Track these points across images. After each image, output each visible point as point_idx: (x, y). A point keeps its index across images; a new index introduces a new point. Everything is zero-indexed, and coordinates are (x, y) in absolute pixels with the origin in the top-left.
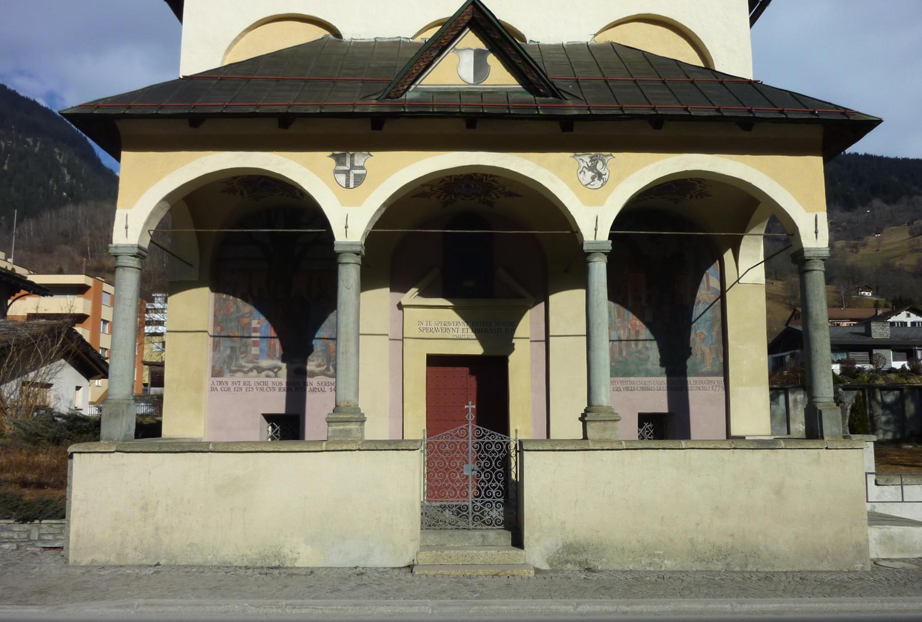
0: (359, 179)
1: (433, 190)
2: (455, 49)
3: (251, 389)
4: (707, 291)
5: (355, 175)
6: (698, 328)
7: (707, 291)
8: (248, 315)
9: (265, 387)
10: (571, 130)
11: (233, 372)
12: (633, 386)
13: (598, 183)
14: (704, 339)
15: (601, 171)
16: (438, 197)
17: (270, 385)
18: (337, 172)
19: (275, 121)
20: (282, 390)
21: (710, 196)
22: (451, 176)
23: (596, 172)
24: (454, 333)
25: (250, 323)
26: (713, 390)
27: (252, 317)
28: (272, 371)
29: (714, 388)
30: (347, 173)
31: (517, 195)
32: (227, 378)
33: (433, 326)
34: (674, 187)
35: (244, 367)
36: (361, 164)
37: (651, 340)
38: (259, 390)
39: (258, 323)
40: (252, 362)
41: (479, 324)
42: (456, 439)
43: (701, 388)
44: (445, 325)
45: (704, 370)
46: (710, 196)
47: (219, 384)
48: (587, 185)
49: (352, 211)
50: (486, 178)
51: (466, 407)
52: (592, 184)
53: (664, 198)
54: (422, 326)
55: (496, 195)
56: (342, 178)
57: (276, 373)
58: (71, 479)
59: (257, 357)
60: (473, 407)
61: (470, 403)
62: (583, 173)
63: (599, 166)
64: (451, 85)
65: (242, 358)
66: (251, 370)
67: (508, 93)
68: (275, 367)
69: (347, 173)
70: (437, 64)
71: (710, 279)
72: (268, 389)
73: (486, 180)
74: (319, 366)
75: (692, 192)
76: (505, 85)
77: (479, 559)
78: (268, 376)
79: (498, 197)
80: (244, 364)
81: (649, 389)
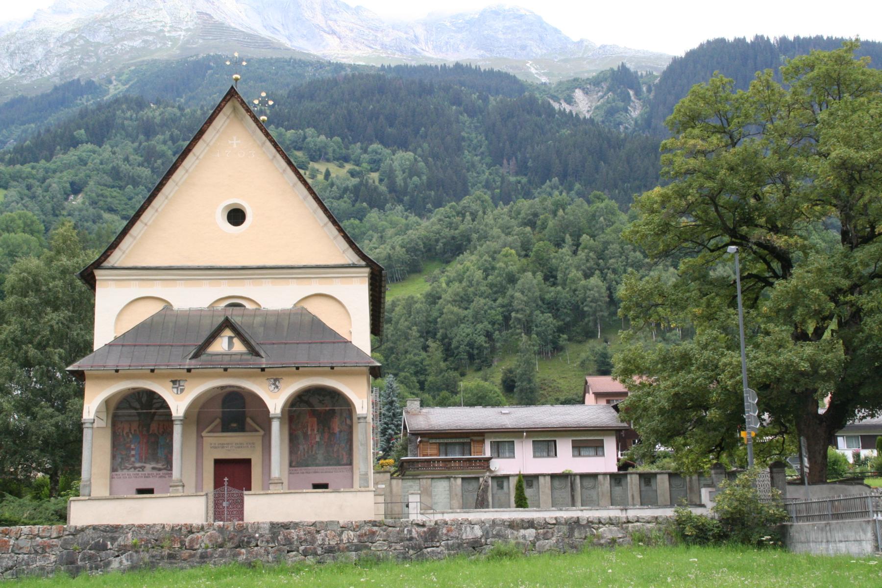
0: (182, 391)
11: (122, 469)
13: (276, 390)
18: (173, 388)
30: (177, 388)
32: (120, 472)
37: (354, 266)
56: (175, 390)
58: (70, 511)
59: (134, 462)
63: (277, 383)
66: (131, 468)
69: (177, 388)
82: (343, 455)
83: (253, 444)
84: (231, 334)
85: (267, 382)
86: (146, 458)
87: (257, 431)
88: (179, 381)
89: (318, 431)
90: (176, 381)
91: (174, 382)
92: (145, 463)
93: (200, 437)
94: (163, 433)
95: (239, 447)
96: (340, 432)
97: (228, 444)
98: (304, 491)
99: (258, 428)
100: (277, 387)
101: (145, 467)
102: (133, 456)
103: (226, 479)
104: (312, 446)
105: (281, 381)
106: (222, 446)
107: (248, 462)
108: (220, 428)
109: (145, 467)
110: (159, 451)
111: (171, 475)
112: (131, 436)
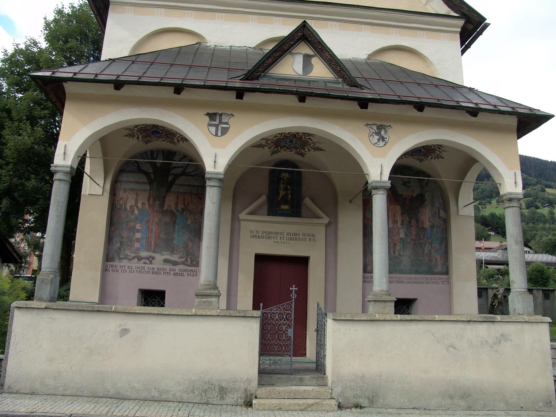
0: (225, 131)
1: (267, 143)
2: (291, 53)
3: (133, 272)
4: (439, 219)
5: (222, 127)
6: (433, 243)
7: (439, 219)
8: (134, 220)
9: (143, 271)
10: (367, 108)
12: (392, 280)
13: (381, 143)
14: (437, 250)
15: (384, 136)
16: (270, 148)
17: (146, 269)
18: (209, 125)
19: (172, 89)
20: (154, 273)
21: (443, 158)
22: (282, 134)
23: (380, 136)
24: (274, 240)
25: (135, 226)
26: (442, 284)
27: (136, 222)
28: (148, 260)
29: (443, 282)
30: (217, 126)
31: (321, 150)
33: (260, 235)
34: (423, 151)
35: (129, 256)
36: (226, 121)
38: (138, 272)
39: (140, 226)
40: (135, 253)
41: (291, 234)
42: (283, 311)
43: (435, 282)
44: (268, 234)
45: (437, 270)
46: (443, 158)
47: (111, 267)
48: (375, 144)
49: (218, 151)
50: (305, 137)
51: (291, 289)
52: (378, 143)
53: (414, 158)
54: (253, 234)
55: (308, 149)
56: (213, 129)
57: (151, 261)
59: (138, 249)
60: (296, 289)
61: (294, 286)
62: (372, 136)
63: (383, 133)
64: (288, 75)
65: (128, 249)
66: (134, 258)
67: (326, 82)
68: (150, 257)
70: (279, 61)
71: (440, 212)
72: (145, 272)
73: (304, 138)
74: (181, 258)
75: (433, 155)
76: (323, 77)
77: (300, 394)
78: (145, 263)
79: (309, 150)
80: (129, 254)
81: (402, 282)
82: (436, 260)
83: (313, 235)
84: (310, 52)
85: (367, 130)
86: (156, 245)
87: (318, 217)
88: (221, 115)
89: (402, 224)
90: (215, 114)
91: (212, 116)
92: (154, 252)
93: (235, 219)
94: (183, 210)
95: (292, 239)
96: (432, 227)
97: (277, 233)
98: (437, 317)
99: (321, 214)
100: (383, 139)
101: (154, 258)
102: (138, 240)
103: (294, 288)
104: (395, 244)
105: (390, 131)
106: (268, 235)
107: (304, 261)
108: (265, 209)
109: (154, 258)
110: (176, 235)
111: (196, 274)
112: (136, 212)
